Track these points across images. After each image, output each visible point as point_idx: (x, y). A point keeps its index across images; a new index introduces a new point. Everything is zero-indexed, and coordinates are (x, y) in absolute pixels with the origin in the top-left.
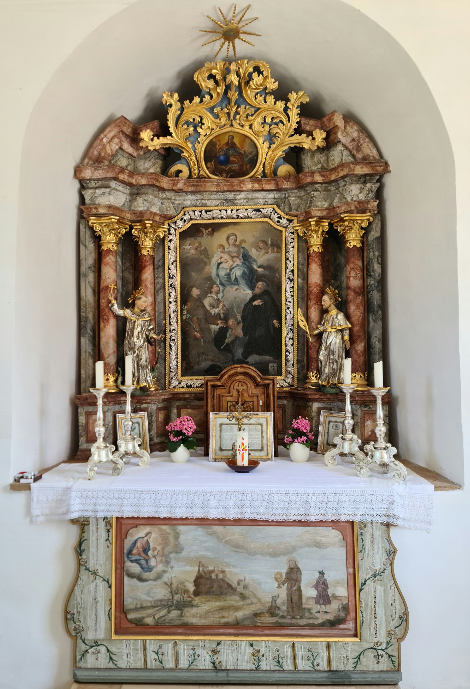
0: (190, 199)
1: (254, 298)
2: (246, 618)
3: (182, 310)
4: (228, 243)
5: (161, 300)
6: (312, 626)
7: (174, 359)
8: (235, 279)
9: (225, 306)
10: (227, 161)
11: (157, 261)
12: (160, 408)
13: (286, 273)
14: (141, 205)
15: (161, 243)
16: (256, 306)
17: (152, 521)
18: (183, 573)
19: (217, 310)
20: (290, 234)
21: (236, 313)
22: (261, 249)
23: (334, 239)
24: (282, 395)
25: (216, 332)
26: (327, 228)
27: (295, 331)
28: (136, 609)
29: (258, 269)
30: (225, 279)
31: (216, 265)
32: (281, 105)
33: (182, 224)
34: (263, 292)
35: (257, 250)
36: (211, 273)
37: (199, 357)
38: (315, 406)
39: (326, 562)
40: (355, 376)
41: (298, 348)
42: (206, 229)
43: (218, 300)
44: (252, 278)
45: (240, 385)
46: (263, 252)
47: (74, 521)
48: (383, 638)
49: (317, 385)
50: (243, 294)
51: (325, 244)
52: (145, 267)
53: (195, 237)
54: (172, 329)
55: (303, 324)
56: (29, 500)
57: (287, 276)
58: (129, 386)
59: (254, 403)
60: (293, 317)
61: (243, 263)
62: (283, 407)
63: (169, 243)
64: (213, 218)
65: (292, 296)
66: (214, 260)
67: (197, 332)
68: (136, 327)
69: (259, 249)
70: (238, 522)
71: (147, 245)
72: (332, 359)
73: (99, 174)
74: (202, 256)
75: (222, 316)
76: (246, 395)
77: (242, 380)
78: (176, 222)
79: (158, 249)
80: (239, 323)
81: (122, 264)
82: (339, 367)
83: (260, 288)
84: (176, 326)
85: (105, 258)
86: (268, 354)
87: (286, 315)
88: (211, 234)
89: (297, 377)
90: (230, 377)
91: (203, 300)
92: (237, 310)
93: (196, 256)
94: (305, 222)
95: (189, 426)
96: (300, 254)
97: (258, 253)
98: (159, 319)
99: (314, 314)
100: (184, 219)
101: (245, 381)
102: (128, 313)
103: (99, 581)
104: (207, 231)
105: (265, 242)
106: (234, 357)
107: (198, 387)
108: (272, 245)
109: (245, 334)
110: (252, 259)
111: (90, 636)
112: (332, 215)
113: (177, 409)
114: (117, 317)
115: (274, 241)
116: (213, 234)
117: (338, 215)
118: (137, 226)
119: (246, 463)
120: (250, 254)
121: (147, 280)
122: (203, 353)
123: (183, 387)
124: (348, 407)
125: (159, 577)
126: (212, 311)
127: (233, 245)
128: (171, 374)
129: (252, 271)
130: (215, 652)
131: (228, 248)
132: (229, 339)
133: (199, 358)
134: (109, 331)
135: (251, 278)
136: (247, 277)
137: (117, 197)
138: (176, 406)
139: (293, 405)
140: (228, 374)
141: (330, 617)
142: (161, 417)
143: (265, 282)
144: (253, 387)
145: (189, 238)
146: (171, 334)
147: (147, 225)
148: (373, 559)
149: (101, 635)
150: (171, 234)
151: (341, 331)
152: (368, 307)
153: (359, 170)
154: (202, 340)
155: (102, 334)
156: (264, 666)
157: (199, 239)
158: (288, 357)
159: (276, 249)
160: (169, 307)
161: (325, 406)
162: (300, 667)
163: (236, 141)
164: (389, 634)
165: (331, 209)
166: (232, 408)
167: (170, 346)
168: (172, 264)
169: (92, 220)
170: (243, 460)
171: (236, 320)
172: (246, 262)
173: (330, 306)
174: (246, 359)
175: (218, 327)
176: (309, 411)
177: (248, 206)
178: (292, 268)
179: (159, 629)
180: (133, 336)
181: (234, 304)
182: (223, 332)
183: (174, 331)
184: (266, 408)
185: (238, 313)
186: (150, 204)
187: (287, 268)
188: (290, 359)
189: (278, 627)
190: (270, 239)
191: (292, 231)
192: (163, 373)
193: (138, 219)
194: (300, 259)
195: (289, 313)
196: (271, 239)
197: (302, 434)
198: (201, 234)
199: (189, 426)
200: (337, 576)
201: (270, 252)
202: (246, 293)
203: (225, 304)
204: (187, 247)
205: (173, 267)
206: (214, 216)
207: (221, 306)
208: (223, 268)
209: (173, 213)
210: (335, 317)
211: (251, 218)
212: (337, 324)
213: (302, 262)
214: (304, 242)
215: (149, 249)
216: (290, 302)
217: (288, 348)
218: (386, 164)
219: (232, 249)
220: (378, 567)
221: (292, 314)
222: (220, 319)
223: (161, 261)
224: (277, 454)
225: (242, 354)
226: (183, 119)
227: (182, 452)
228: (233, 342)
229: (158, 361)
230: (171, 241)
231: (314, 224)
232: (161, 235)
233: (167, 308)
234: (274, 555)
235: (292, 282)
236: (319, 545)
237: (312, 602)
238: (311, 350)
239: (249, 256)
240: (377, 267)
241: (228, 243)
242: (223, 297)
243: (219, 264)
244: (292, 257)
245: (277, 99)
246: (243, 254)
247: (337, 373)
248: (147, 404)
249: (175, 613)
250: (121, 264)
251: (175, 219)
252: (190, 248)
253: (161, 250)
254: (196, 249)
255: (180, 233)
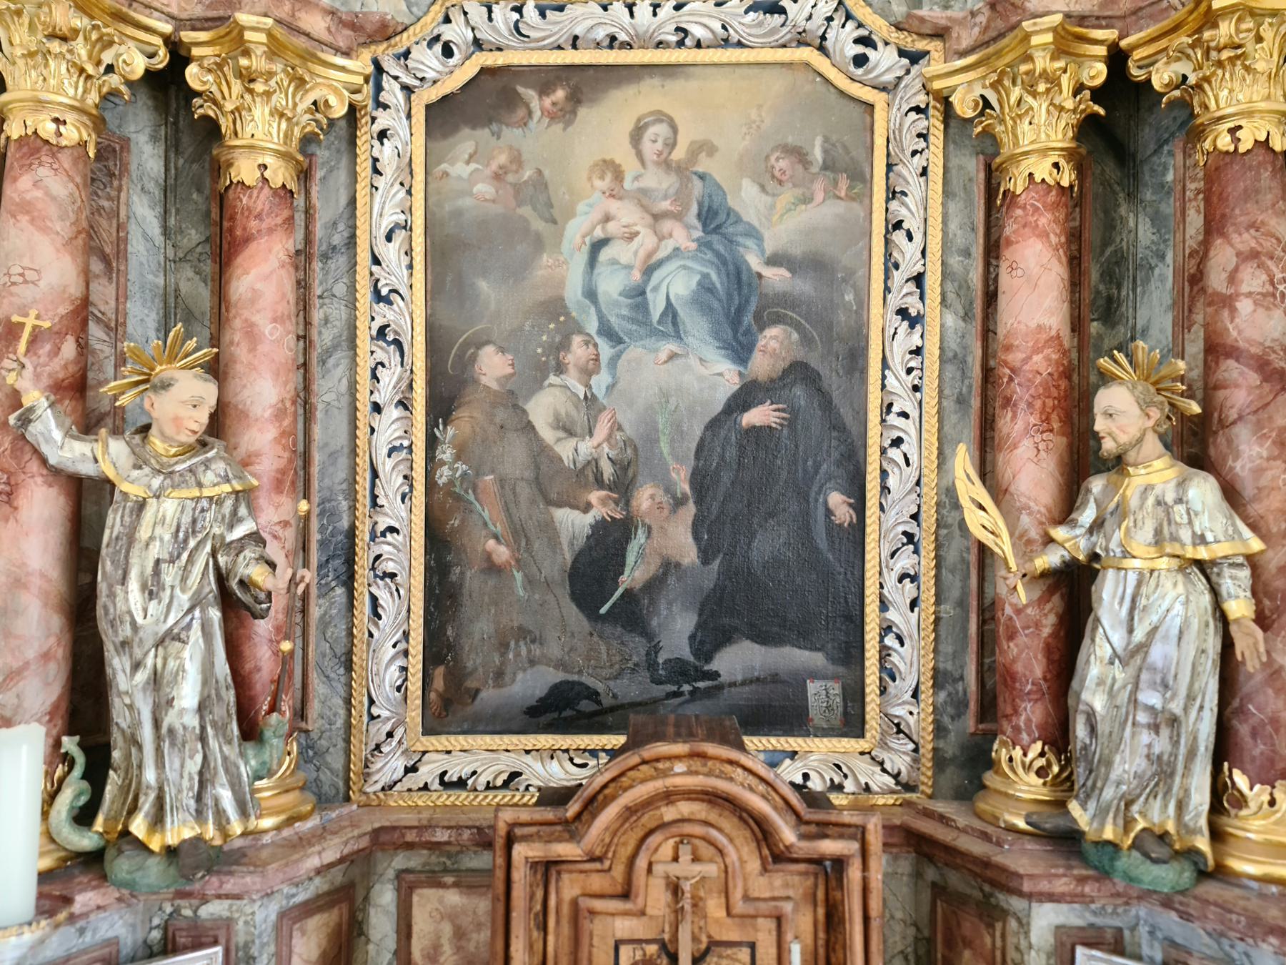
3: (432, 443)
4: (640, 155)
5: (339, 395)
8: (664, 314)
9: (620, 428)
11: (325, 227)
12: (305, 904)
13: (887, 289)
16: (753, 429)
19: (586, 447)
20: (913, 115)
21: (669, 459)
22: (780, 182)
25: (581, 542)
26: (1099, 73)
27: (927, 546)
29: (768, 272)
30: (625, 312)
31: (586, 249)
33: (436, 64)
34: (786, 372)
35: (763, 188)
36: (561, 284)
37: (503, 646)
40: (1272, 803)
41: (937, 622)
42: (544, 90)
43: (590, 399)
44: (740, 311)
45: (685, 856)
46: (788, 195)
50: (701, 379)
52: (247, 240)
53: (494, 127)
54: (381, 528)
57: (895, 301)
59: (760, 952)
60: (918, 483)
61: (703, 245)
63: (376, 143)
64: (575, 42)
65: (916, 388)
66: (577, 230)
67: (496, 537)
68: (143, 533)
69: (771, 185)
71: (260, 141)
72: (1151, 709)
74: (526, 211)
75: (608, 471)
76: (715, 907)
77: (698, 830)
78: (406, 54)
79: (331, 171)
80: (679, 502)
81: (166, 231)
82: (1183, 750)
83: (774, 354)
84: (401, 514)
85: (15, 180)
86: (804, 638)
87: (884, 473)
88: (565, 114)
89: (935, 750)
90: (631, 812)
91: (528, 397)
92: (673, 448)
93: (498, 209)
96: (952, 207)
97: (769, 199)
98: (327, 482)
100: (444, 38)
101: (714, 833)
102: (108, 456)
104: (547, 102)
105: (799, 155)
106: (656, 649)
107: (495, 788)
108: (825, 167)
109: (706, 556)
110: (740, 228)
113: (398, 890)
116: (574, 112)
120: (731, 202)
121: (253, 301)
122: (523, 633)
123: (426, 787)
126: (566, 450)
127: (658, 164)
128: (373, 729)
129: (739, 277)
131: (636, 178)
132: (637, 574)
133: (503, 655)
135: (738, 310)
136: (716, 305)
138: (391, 874)
139: (917, 875)
140: (626, 799)
143: (797, 327)
144: (754, 865)
145: (466, 131)
146: (376, 550)
147: (248, 35)
150: (386, 107)
154: (519, 576)
157: (511, 135)
158: (895, 658)
159: (843, 184)
160: (373, 430)
161: (1092, 919)
167: (374, 600)
168: (389, 238)
171: (667, 490)
172: (715, 238)
173: (1140, 441)
174: (709, 658)
175: (589, 519)
176: (1011, 940)
178: (919, 268)
180: (124, 581)
181: (661, 421)
182: (609, 542)
183: (389, 537)
185: (677, 459)
187: (891, 265)
188: (902, 666)
190: (818, 141)
191: (921, 100)
192: (340, 722)
193: (211, 14)
194: (953, 226)
195: (902, 462)
196: (826, 140)
198: (521, 112)
201: (819, 196)
202: (712, 375)
203: (620, 418)
204: (460, 169)
205: (391, 253)
206: (578, 31)
207: (602, 430)
208: (614, 262)
209: (399, 12)
210: (1169, 498)
211: (740, 44)
212: (1186, 535)
213: (960, 240)
214: (976, 141)
215: (269, 160)
216: (905, 415)
217: (892, 615)
219: (656, 180)
222: (599, 483)
223: (341, 227)
225: (692, 638)
228: (654, 585)
230: (382, 135)
231: (1043, 46)
232: (333, 101)
233: (363, 432)
235: (918, 327)
238: (1011, 637)
239: (729, 212)
241: (640, 155)
242: (611, 388)
243: (598, 246)
244: (928, 211)
246: (700, 205)
247: (1172, 775)
248: (227, 903)
250: (155, 229)
251: (403, 41)
252: (472, 166)
253: (342, 176)
254: (498, 177)
255: (429, 107)
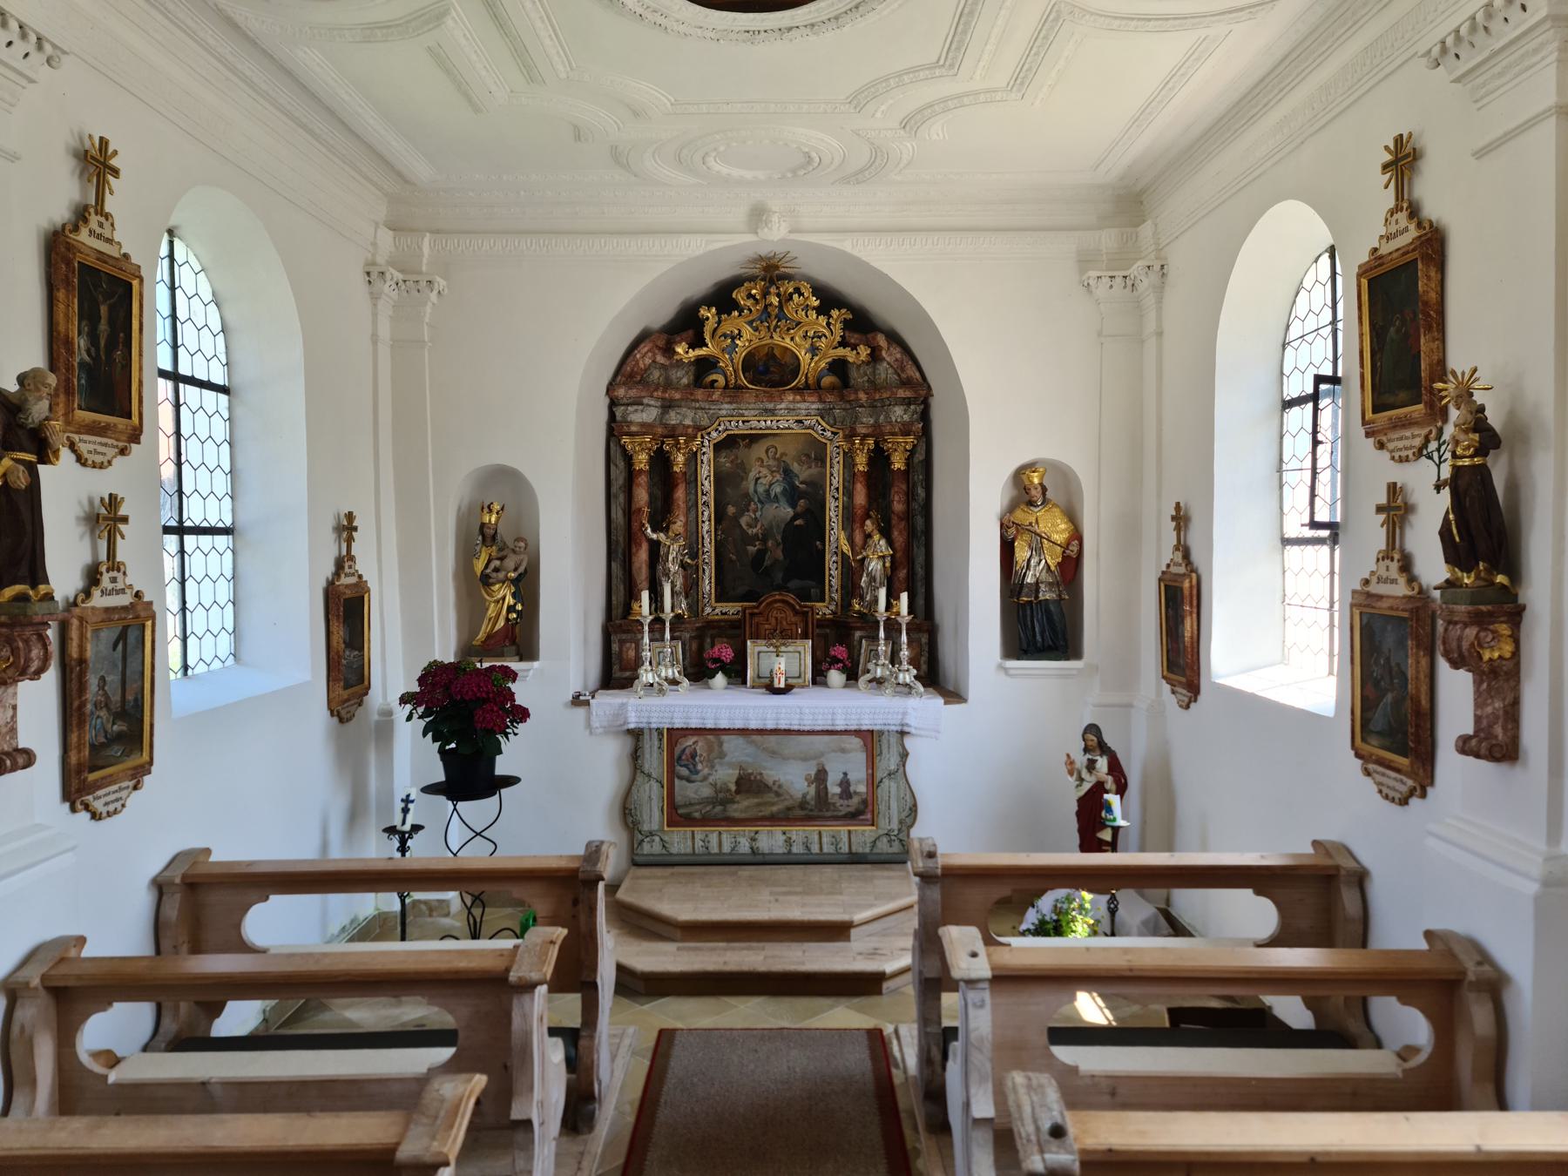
0: (726, 408)
1: (795, 518)
2: (779, 812)
6: (836, 818)
7: (708, 585)
10: (767, 371)
14: (673, 418)
15: (693, 458)
17: (700, 731)
18: (725, 775)
23: (879, 458)
24: (822, 623)
28: (685, 806)
32: (822, 320)
38: (858, 634)
39: (849, 765)
47: (629, 731)
48: (895, 825)
49: (859, 612)
51: (871, 462)
55: (846, 548)
56: (589, 714)
58: (668, 614)
62: (826, 637)
66: (752, 475)
70: (776, 732)
73: (633, 393)
84: (709, 546)
88: (749, 446)
94: (849, 437)
95: (727, 654)
99: (858, 538)
102: (662, 537)
103: (653, 782)
111: (645, 828)
112: (878, 433)
114: (651, 541)
115: (816, 453)
117: (883, 434)
118: (670, 441)
119: (782, 685)
124: (882, 634)
125: (705, 779)
129: (793, 487)
130: (753, 839)
134: (642, 555)
135: (792, 495)
137: (648, 415)
141: (851, 809)
142: (694, 646)
148: (889, 761)
149: (655, 827)
151: (883, 557)
152: (911, 533)
153: (901, 393)
155: (634, 559)
156: (795, 850)
162: (825, 850)
163: (777, 352)
164: (901, 822)
165: (877, 425)
166: (768, 637)
169: (625, 439)
170: (781, 683)
177: (789, 418)
179: (705, 821)
182: (761, 553)
184: (805, 636)
186: (682, 417)
189: (808, 819)
197: (839, 661)
199: (727, 654)
200: (858, 775)
205: (706, 483)
218: (929, 387)
219: (771, 462)
220: (893, 767)
221: (837, 537)
224: (814, 682)
226: (719, 332)
227: (720, 679)
229: (691, 588)
234: (805, 759)
236: (843, 751)
237: (836, 799)
240: (921, 492)
245: (819, 314)
249: (718, 809)
